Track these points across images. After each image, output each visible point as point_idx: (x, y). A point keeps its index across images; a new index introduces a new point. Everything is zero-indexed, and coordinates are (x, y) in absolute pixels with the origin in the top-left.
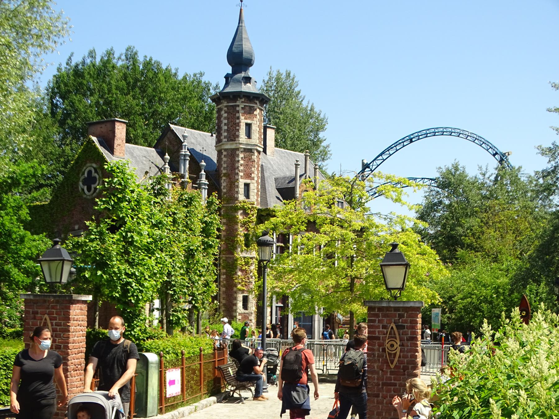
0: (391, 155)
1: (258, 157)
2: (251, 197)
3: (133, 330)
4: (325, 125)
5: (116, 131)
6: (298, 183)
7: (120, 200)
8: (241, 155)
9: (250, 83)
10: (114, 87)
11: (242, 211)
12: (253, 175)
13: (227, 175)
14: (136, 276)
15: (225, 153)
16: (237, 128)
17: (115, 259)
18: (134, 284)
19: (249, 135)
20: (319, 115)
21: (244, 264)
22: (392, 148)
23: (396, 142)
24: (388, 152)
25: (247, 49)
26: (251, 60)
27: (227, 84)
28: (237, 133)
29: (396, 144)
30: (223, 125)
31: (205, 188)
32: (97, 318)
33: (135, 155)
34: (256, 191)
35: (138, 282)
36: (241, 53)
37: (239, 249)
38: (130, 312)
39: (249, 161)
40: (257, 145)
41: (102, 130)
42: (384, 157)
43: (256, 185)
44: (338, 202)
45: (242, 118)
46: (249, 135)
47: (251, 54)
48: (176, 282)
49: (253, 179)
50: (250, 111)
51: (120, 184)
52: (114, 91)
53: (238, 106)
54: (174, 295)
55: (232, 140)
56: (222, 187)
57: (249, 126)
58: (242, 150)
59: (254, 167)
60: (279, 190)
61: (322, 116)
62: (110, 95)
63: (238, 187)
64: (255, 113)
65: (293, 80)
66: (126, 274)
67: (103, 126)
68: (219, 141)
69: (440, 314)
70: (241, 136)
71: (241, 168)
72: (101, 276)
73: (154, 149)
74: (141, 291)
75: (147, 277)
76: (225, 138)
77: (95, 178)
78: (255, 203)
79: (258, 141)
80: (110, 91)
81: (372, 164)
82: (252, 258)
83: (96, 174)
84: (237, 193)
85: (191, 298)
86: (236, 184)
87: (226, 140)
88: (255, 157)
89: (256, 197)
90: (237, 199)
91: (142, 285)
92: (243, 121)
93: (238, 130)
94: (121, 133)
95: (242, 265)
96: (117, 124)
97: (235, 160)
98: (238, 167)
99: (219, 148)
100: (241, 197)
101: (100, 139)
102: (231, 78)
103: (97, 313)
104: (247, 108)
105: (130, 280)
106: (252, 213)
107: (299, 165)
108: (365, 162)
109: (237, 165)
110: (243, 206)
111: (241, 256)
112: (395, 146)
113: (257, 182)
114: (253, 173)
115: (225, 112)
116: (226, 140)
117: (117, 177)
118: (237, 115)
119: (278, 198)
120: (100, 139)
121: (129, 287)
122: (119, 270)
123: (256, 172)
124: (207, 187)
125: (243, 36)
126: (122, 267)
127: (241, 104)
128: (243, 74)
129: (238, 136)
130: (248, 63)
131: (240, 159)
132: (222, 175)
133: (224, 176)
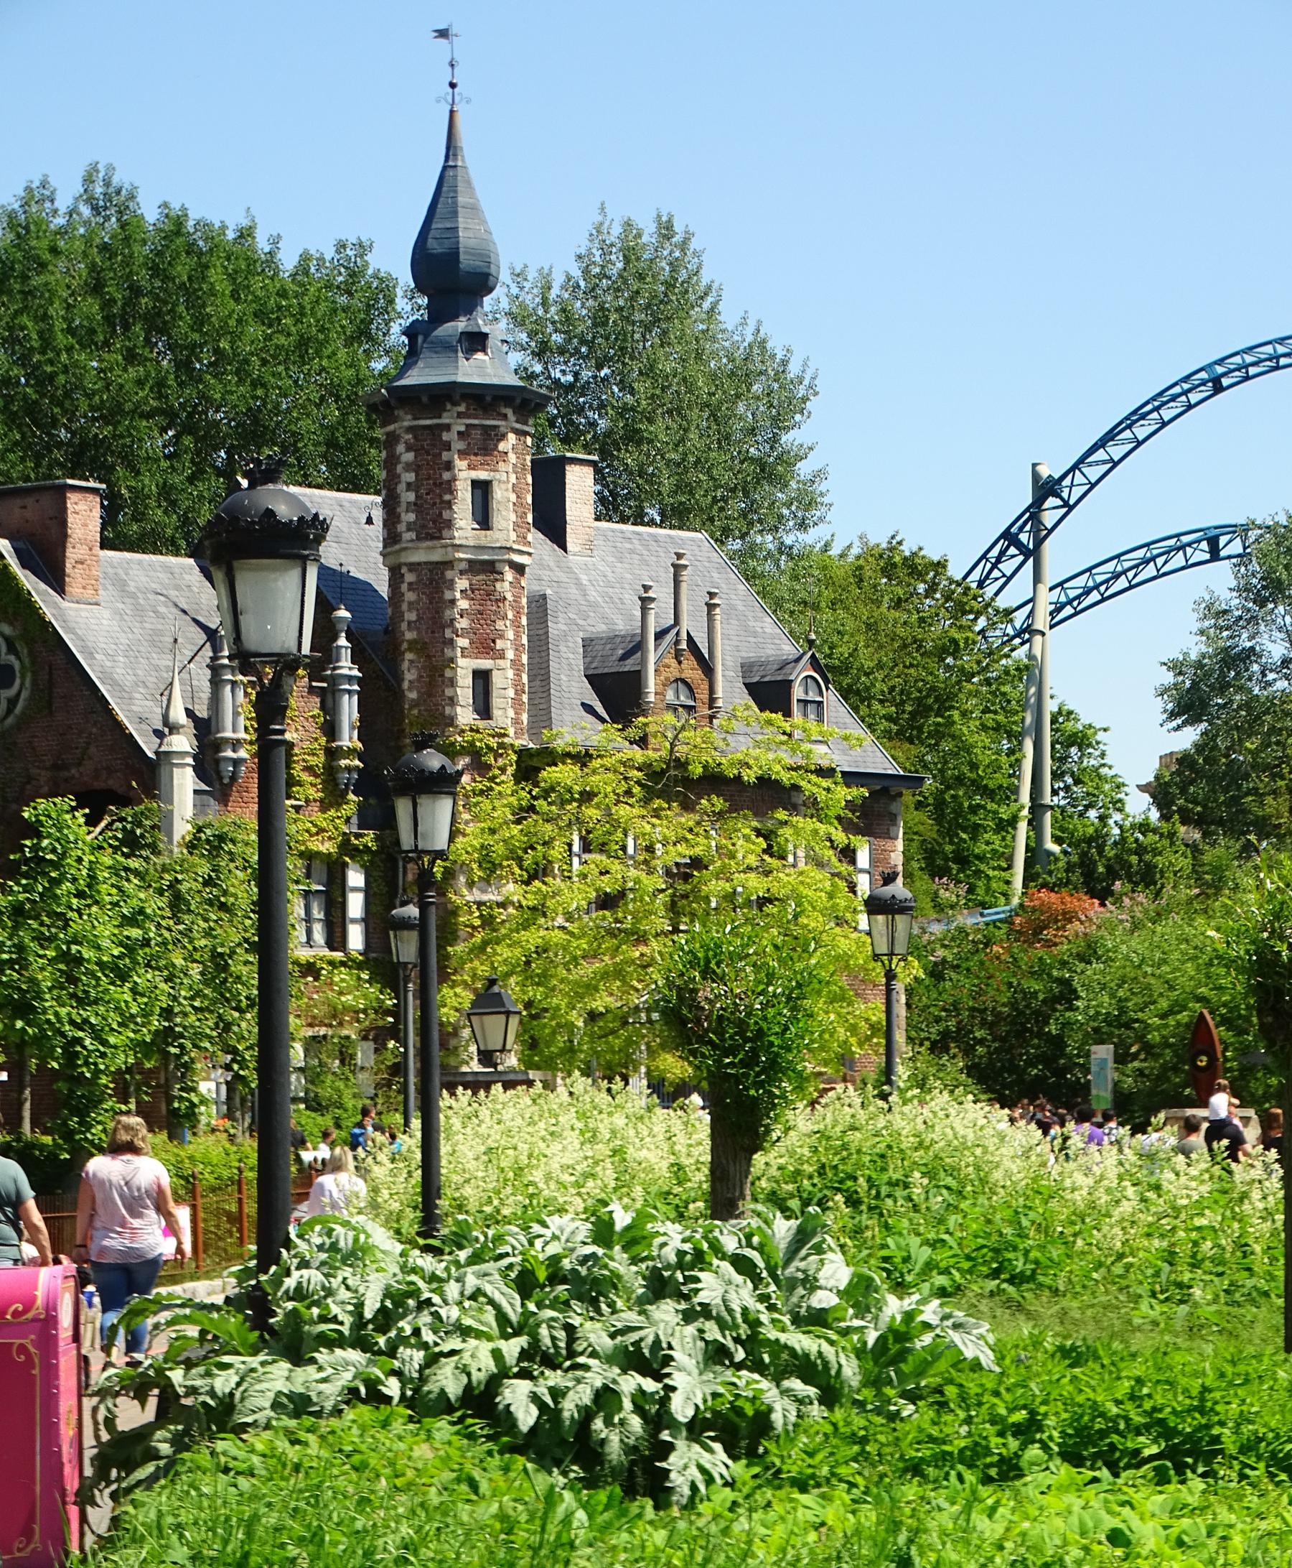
0: (1139, 444)
1: (515, 584)
2: (496, 713)
3: (88, 1130)
4: (805, 400)
5: (71, 519)
6: (652, 658)
7: (56, 882)
8: (462, 583)
9: (484, 350)
10: (59, 325)
11: (467, 760)
12: (500, 644)
13: (419, 647)
14: (92, 1026)
15: (410, 577)
16: (447, 497)
17: (47, 996)
18: (87, 1042)
19: (483, 518)
20: (785, 363)
21: (477, 922)
22: (1143, 417)
23: (1161, 394)
24: (1127, 434)
25: (472, 243)
26: (488, 275)
27: (413, 354)
28: (446, 515)
29: (1160, 399)
30: (401, 488)
31: (349, 692)
32: (28, 1105)
33: (132, 587)
34: (511, 693)
35: (97, 1036)
36: (454, 255)
37: (462, 879)
38: (83, 1096)
39: (487, 598)
40: (510, 549)
41: (28, 514)
42: (1116, 451)
43: (510, 674)
44: (805, 702)
45: (460, 464)
46: (483, 518)
47: (486, 257)
48: (185, 1027)
49: (502, 657)
50: (484, 446)
51: (54, 851)
52: (61, 340)
53: (448, 427)
54: (182, 1054)
55: (433, 538)
56: (406, 685)
57: (482, 490)
58: (464, 566)
59: (505, 617)
60: (596, 681)
61: (794, 369)
62: (51, 355)
63: (452, 683)
64: (502, 446)
65: (684, 246)
66: (72, 1022)
67: (29, 501)
68: (391, 538)
69: (1111, 1064)
70: (460, 523)
71: (463, 623)
72: (23, 1029)
73: (191, 561)
74: (103, 1055)
75: (115, 1026)
76: (409, 530)
77: (10, 668)
78: (511, 731)
79: (513, 536)
80: (47, 341)
81: (1067, 482)
82: (502, 905)
83: (12, 658)
84: (452, 701)
85: (229, 1057)
86: (448, 673)
87: (413, 535)
88: (506, 584)
89: (511, 713)
90: (451, 721)
91: (104, 1043)
92: (464, 474)
93: (449, 505)
94: (85, 525)
95: (474, 928)
96: (72, 498)
97: (441, 599)
98: (453, 620)
99: (392, 560)
100: (465, 715)
101: (21, 545)
102: (426, 336)
103: (27, 1092)
104: (477, 434)
105: (81, 1034)
106: (501, 762)
107: (653, 600)
108: (1045, 472)
109: (447, 613)
110: (472, 743)
111: (470, 898)
112: (1157, 409)
113: (516, 663)
114: (502, 637)
115: (409, 449)
116: (413, 535)
117: (49, 836)
118: (445, 456)
119: (589, 709)
120: (21, 545)
121: (79, 1049)
122: (56, 1014)
123: (510, 634)
124: (356, 687)
125: (461, 200)
126: (63, 1011)
127: (455, 421)
128: (461, 325)
129: (449, 524)
130: (482, 283)
131: (458, 595)
132: (405, 645)
133: (410, 649)
